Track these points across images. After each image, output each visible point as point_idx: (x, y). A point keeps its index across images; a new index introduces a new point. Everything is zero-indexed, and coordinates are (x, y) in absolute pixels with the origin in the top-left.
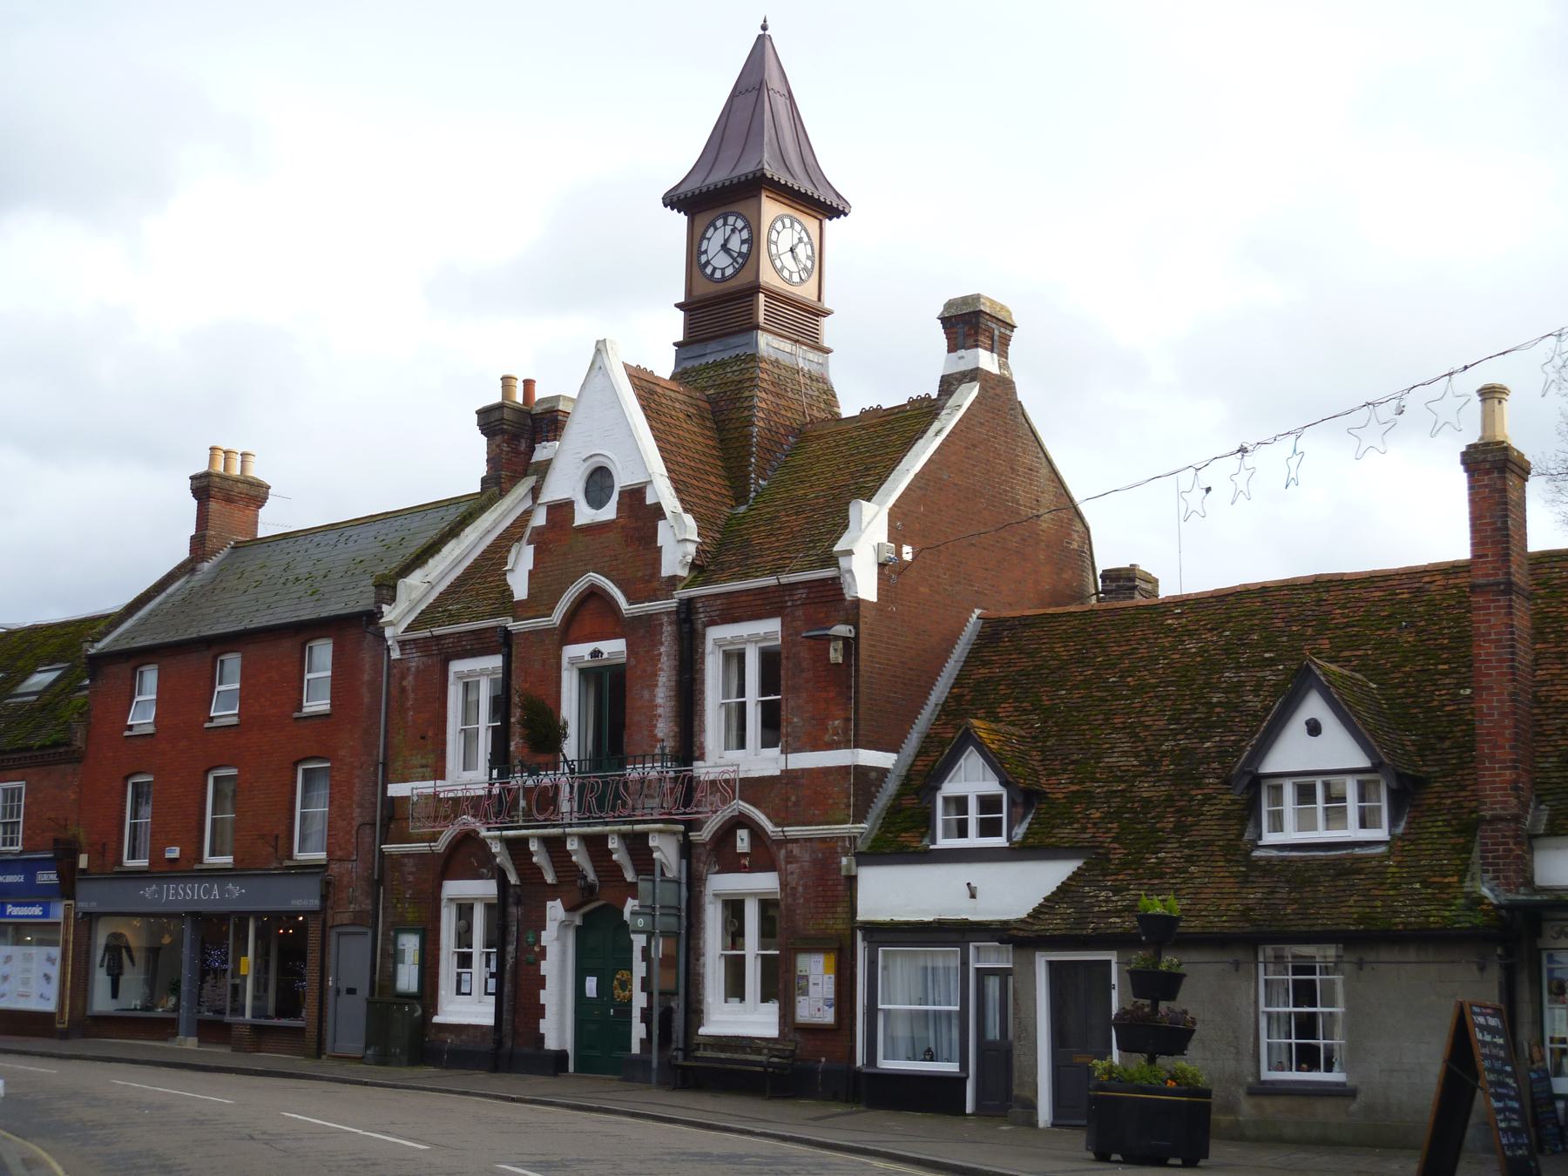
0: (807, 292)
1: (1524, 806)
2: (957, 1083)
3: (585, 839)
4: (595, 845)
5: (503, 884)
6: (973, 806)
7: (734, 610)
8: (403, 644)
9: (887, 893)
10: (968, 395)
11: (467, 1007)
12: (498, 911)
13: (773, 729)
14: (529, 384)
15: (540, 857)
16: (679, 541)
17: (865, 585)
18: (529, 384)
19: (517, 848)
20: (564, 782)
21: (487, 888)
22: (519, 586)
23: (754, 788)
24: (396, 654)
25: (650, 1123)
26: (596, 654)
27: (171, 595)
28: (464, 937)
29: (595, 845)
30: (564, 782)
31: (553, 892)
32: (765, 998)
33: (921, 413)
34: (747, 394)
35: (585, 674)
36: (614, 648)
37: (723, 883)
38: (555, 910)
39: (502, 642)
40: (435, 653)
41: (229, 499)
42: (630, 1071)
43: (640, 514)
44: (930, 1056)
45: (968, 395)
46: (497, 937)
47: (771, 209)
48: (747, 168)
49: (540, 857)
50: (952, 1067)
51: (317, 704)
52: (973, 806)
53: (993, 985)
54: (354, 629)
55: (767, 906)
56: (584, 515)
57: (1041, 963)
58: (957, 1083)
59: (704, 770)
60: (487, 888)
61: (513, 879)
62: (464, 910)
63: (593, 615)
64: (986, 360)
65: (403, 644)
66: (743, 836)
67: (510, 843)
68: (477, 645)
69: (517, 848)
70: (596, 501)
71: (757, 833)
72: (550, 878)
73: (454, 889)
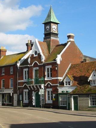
0: (56, 32)
1: (56, 50)
4: (36, 86)
6: (68, 82)
7: (48, 64)
8: (19, 67)
10: (69, 43)
11: (26, 101)
12: (28, 92)
14: (31, 41)
15: (32, 88)
17: (58, 62)
18: (31, 41)
19: (30, 87)
20: (33, 80)
21: (27, 90)
23: (49, 81)
24: (19, 68)
26: (36, 68)
27: (42, 50)
29: (36, 86)
30: (33, 80)
31: (33, 91)
32: (51, 100)
35: (35, 70)
36: (38, 68)
37: (48, 90)
39: (28, 67)
40: (22, 69)
41: (3, 52)
43: (40, 56)
44: (64, 105)
45: (69, 43)
46: (28, 95)
47: (52, 24)
48: (49, 21)
49: (32, 88)
50: (66, 106)
51: (12, 73)
52: (68, 82)
54: (15, 65)
55: (51, 68)
56: (35, 56)
57: (72, 96)
59: (46, 79)
60: (27, 90)
61: (30, 89)
62: (26, 92)
63: (36, 65)
64: (71, 40)
65: (19, 67)
68: (26, 68)
69: (30, 87)
70: (36, 54)
71: (50, 85)
72: (33, 89)
73: (25, 90)
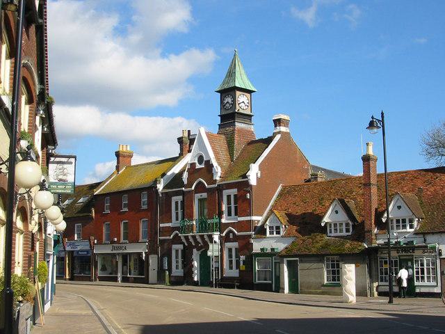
0: (248, 112)
2: (271, 285)
3: (200, 236)
4: (202, 237)
5: (184, 245)
7: (229, 186)
8: (162, 193)
9: (257, 246)
10: (278, 137)
12: (183, 251)
13: (236, 214)
14: (189, 131)
15: (191, 240)
16: (218, 173)
17: (253, 181)
18: (189, 131)
19: (186, 238)
20: (195, 223)
21: (180, 247)
22: (185, 181)
23: (232, 225)
25: (367, 311)
28: (177, 257)
29: (202, 237)
30: (195, 223)
31: (194, 247)
33: (268, 141)
34: (142, 228)
36: (205, 195)
37: (228, 245)
38: (195, 250)
39: (183, 193)
42: (210, 284)
43: (209, 166)
44: (265, 280)
45: (278, 137)
46: (183, 256)
47: (238, 93)
48: (231, 85)
49: (191, 240)
51: (145, 207)
53: (410, 257)
56: (198, 166)
57: (285, 260)
58: (271, 285)
59: (223, 221)
60: (180, 247)
61: (186, 244)
62: (177, 251)
63: (200, 188)
64: (283, 129)
65: (162, 193)
66: (231, 234)
67: (185, 237)
68: (177, 194)
69: (186, 238)
70: (200, 163)
72: (193, 244)
